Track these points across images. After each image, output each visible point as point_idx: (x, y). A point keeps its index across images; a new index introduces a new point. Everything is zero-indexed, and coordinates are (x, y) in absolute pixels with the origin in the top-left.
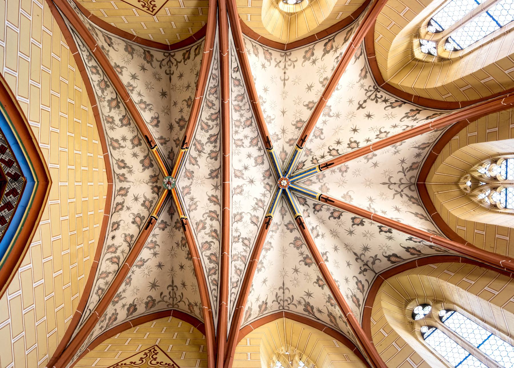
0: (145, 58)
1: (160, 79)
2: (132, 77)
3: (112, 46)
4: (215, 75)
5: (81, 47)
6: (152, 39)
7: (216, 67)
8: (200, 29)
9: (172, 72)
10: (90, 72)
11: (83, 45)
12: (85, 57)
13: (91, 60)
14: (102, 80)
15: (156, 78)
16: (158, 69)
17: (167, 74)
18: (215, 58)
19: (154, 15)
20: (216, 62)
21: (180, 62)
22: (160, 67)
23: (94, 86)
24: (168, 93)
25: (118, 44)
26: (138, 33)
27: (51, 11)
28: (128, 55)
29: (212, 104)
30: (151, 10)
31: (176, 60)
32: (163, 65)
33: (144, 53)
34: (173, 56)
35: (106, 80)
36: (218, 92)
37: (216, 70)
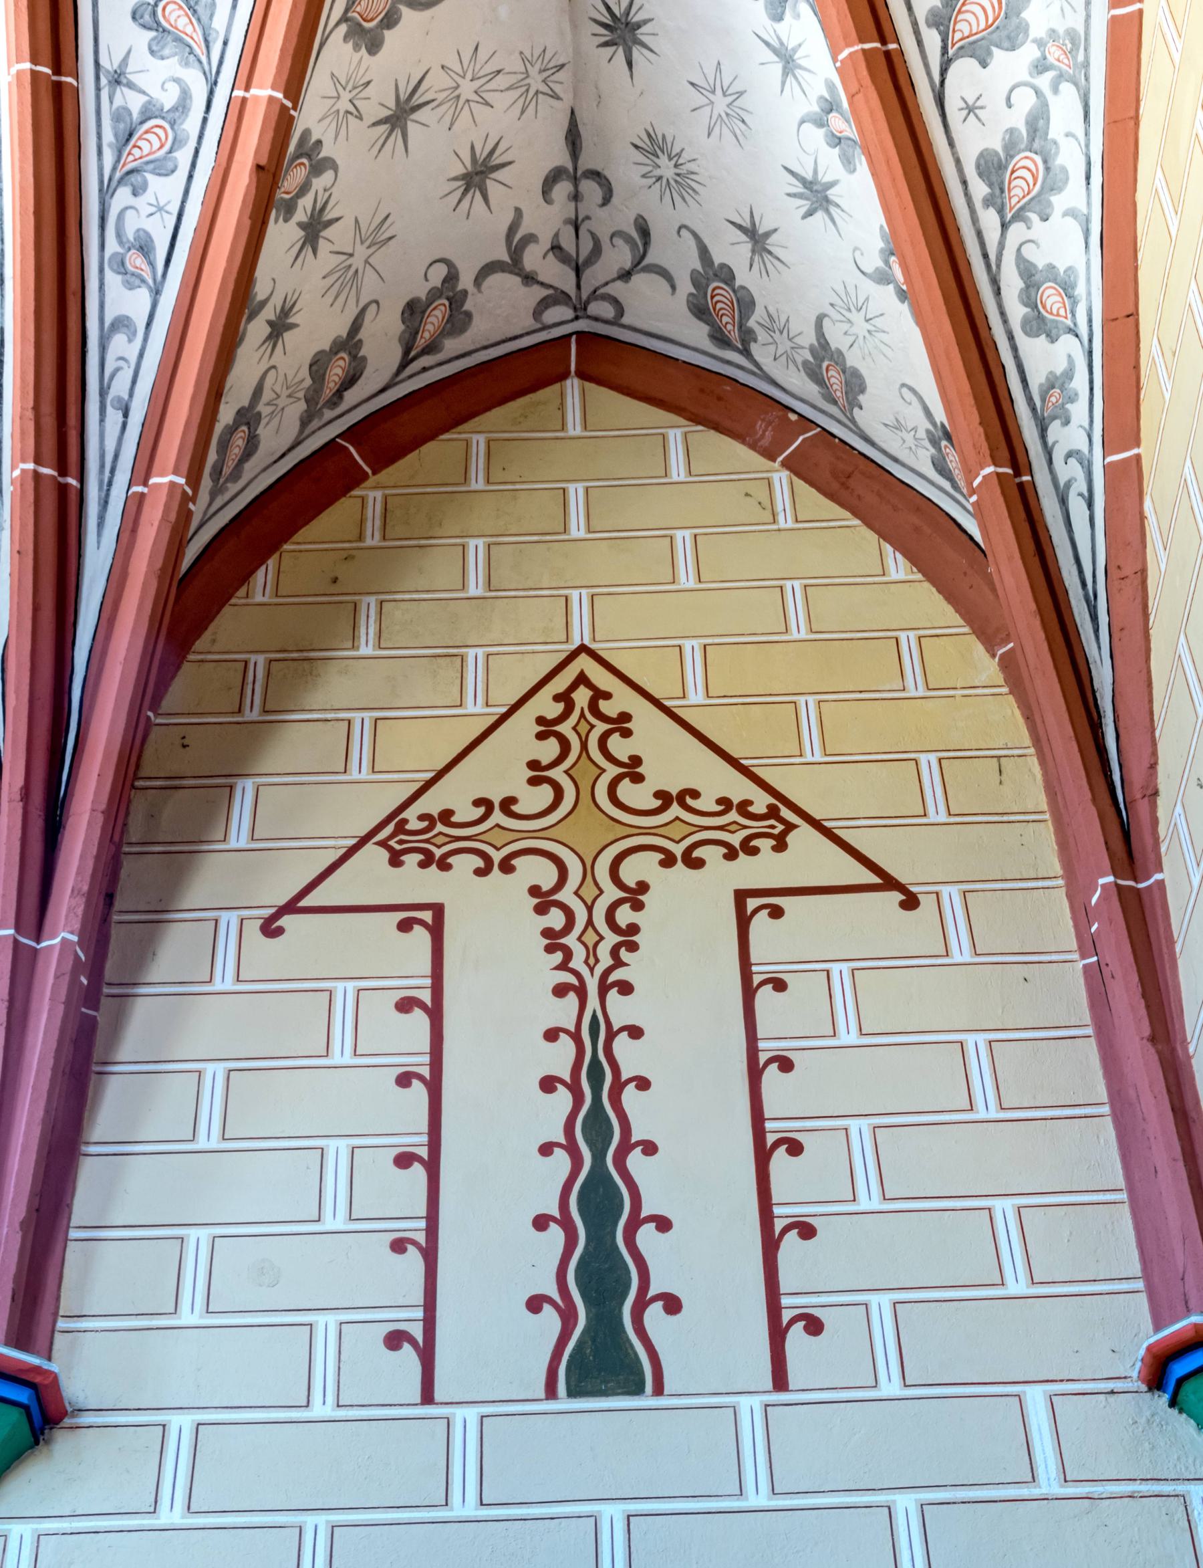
0: (746, 304)
1: (645, 143)
2: (827, 200)
3: (934, 424)
4: (132, 280)
5: (1081, 486)
6: (677, 433)
7: (120, 345)
8: (298, 537)
9: (562, 189)
10: (1080, 290)
11: (1063, 501)
12: (1079, 411)
13: (1054, 383)
14: (1019, 216)
15: (675, 158)
16: (662, 221)
17: (595, 175)
18: (126, 415)
19: (583, 649)
20: (119, 387)
21: (490, 268)
22: (645, 233)
23: (1088, 178)
24: (591, 36)
25: (898, 426)
26: (751, 487)
27: (1153, 766)
28: (844, 350)
29: (157, 26)
30: (582, 697)
31: (529, 279)
32: (628, 239)
33: (747, 337)
34: (558, 297)
35: (990, 220)
36: (108, 136)
37: (122, 323)
